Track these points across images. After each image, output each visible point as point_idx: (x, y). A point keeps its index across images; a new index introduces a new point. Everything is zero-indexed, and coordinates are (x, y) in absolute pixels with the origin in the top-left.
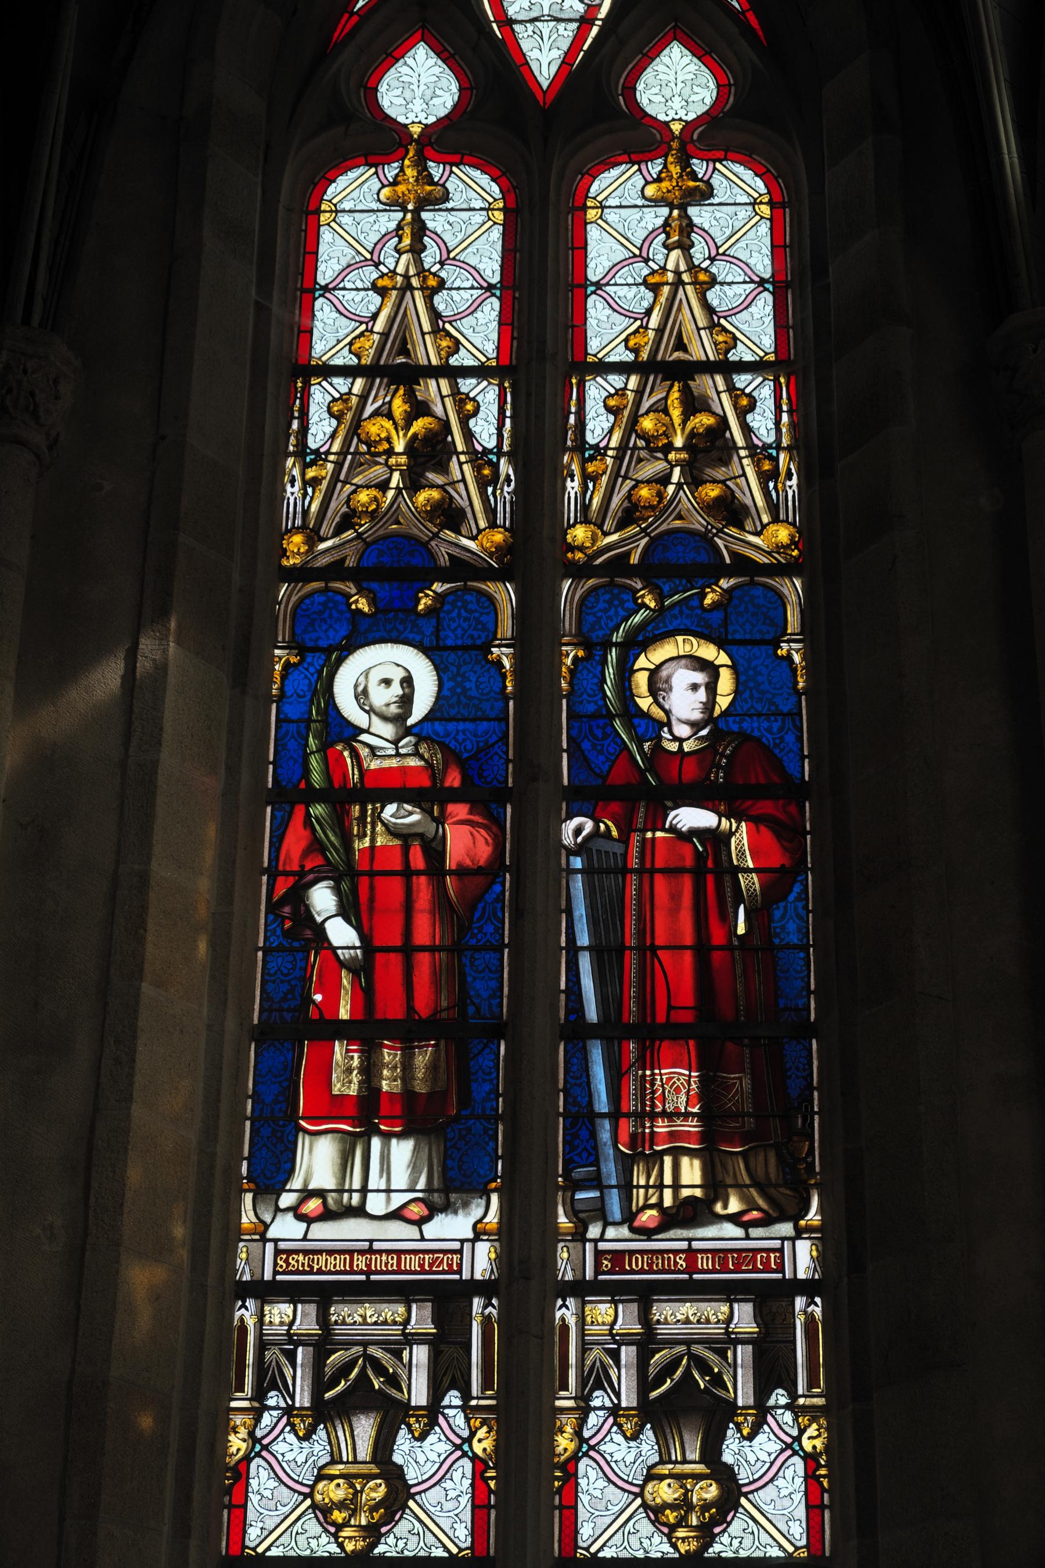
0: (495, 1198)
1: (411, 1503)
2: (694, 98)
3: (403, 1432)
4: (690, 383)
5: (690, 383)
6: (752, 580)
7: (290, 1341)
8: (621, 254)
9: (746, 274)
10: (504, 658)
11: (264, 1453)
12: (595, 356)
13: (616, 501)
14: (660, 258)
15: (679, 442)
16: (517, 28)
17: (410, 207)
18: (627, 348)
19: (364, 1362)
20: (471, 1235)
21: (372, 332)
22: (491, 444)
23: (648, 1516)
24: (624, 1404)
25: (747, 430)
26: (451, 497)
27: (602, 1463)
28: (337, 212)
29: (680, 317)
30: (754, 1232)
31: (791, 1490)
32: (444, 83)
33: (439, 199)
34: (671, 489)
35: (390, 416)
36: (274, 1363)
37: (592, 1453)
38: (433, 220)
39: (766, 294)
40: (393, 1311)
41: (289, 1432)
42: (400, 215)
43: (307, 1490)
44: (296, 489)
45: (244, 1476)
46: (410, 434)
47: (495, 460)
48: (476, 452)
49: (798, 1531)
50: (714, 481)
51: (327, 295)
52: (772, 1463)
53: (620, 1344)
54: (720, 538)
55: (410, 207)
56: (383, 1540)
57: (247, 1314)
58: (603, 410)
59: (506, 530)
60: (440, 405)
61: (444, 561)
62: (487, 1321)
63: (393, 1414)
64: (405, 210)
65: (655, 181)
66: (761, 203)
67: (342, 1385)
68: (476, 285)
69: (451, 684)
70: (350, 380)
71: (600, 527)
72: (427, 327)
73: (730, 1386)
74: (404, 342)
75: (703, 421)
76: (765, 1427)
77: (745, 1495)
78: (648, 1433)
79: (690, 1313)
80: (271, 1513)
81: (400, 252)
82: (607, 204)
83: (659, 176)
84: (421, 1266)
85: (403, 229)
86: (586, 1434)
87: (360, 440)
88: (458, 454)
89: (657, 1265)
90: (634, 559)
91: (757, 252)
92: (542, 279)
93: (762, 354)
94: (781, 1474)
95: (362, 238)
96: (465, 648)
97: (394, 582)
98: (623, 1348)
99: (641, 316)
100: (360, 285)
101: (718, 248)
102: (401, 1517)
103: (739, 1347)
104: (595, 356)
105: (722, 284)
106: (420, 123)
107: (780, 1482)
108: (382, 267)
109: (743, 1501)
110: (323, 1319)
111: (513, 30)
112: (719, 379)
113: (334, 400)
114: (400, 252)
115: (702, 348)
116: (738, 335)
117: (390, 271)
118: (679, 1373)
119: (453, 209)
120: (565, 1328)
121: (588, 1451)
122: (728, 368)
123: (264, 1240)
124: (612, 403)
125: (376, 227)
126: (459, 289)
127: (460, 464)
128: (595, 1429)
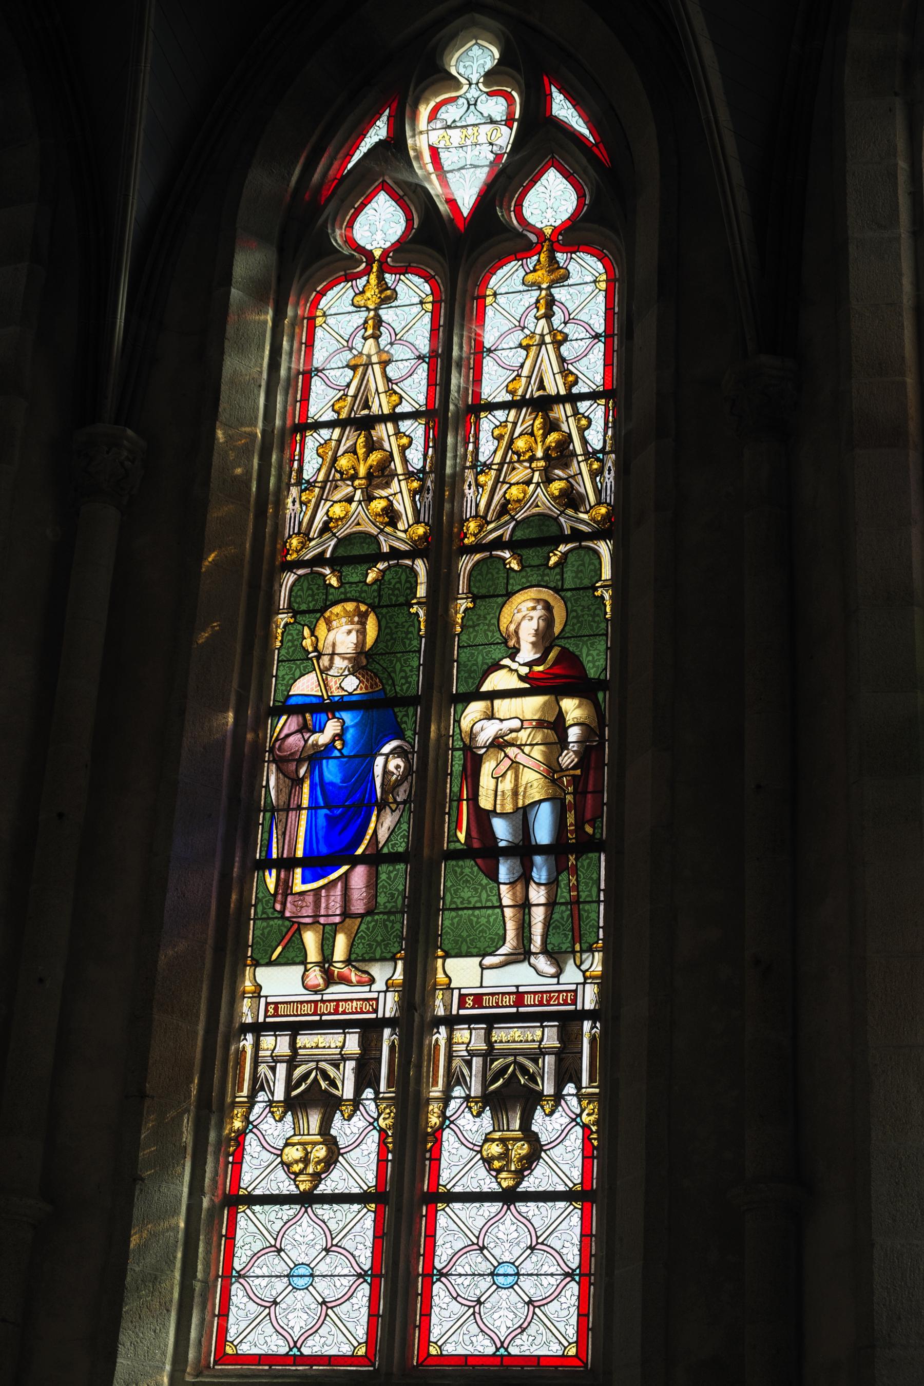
0: (400, 964)
1: (340, 1158)
3: (338, 1115)
13: (496, 498)
15: (539, 454)
18: (333, 410)
20: (582, 981)
21: (347, 395)
24: (472, 1095)
25: (584, 442)
26: (572, 485)
32: (567, 195)
36: (263, 1075)
43: (279, 1152)
44: (472, 490)
48: (589, 453)
50: (381, 498)
51: (320, 374)
52: (563, 1131)
53: (276, 1062)
55: (544, 286)
59: (609, 504)
61: (385, 549)
63: (329, 1104)
64: (540, 289)
65: (531, 272)
67: (303, 1087)
69: (411, 629)
70: (507, 412)
72: (556, 370)
74: (542, 381)
78: (487, 1113)
79: (517, 1035)
81: (365, 339)
83: (534, 268)
86: (251, 1118)
87: (513, 453)
88: (577, 456)
90: (328, 555)
98: (474, 1059)
103: (547, 1057)
108: (354, 351)
109: (543, 1154)
110: (293, 1045)
112: (568, 407)
114: (365, 339)
116: (580, 375)
119: (568, 285)
122: (572, 399)
123: (260, 997)
125: (522, 303)
126: (577, 340)
127: (579, 463)
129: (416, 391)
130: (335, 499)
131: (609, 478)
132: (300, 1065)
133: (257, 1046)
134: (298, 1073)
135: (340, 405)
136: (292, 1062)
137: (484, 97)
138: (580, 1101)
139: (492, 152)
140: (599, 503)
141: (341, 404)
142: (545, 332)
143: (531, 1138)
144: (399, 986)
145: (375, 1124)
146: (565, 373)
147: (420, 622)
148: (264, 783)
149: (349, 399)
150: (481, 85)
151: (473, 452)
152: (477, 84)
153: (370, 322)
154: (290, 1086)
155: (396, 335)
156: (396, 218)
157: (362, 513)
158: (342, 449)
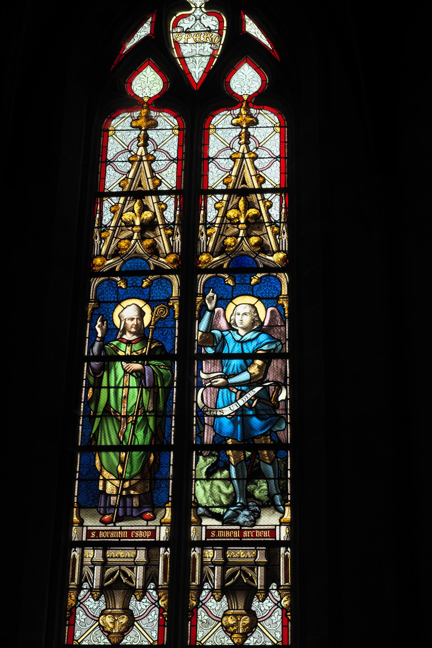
2: (154, 88)
4: (143, 200)
5: (143, 200)
6: (161, 276)
7: (213, 564)
8: (120, 149)
9: (167, 156)
10: (284, 302)
11: (203, 606)
12: (108, 189)
13: (112, 246)
14: (135, 150)
15: (242, 220)
16: (186, 59)
17: (143, 128)
18: (120, 186)
19: (240, 572)
20: (159, 524)
22: (277, 219)
23: (100, 629)
26: (263, 240)
27: (85, 609)
28: (115, 130)
29: (244, 171)
30: (150, 523)
31: (277, 620)
33: (154, 125)
34: (133, 242)
35: (133, 211)
36: (86, 572)
37: (203, 606)
38: (151, 134)
39: (277, 162)
40: (130, 553)
41: (212, 599)
42: (240, 130)
45: (74, 613)
46: (246, 216)
47: (173, 227)
49: (154, 634)
50: (256, 236)
53: (95, 565)
54: (151, 260)
56: (125, 638)
57: (76, 554)
58: (214, 209)
60: (152, 206)
62: (286, 558)
64: (242, 128)
66: (175, 129)
68: (167, 159)
70: (119, 198)
71: (212, 255)
72: (149, 176)
73: (134, 581)
74: (140, 182)
75: (252, 212)
76: (268, 597)
77: (136, 621)
78: (225, 598)
79: (121, 554)
80: (84, 628)
82: (218, 127)
84: (263, 535)
85: (241, 135)
88: (265, 223)
89: (235, 535)
90: (225, 266)
91: (274, 145)
92: (193, 157)
93: (275, 185)
94: (273, 614)
95: (226, 139)
96: (107, 302)
97: (136, 276)
99: (229, 171)
100: (123, 160)
101: (157, 146)
102: (132, 630)
104: (211, 187)
105: (260, 158)
106: (247, 94)
107: (273, 618)
108: (233, 150)
110: (224, 555)
111: (185, 60)
113: (113, 206)
114: (240, 144)
115: (252, 183)
117: (237, 151)
118: (116, 576)
120: (195, 559)
121: (202, 605)
122: (263, 191)
124: (217, 206)
125: (130, 137)
126: (161, 160)
128: (83, 596)
129: (170, 178)
130: (121, 237)
131: (178, 239)
132: (109, 568)
133: (202, 555)
134: (108, 572)
135: (227, 180)
136: (104, 565)
137: (205, 15)
138: (157, 593)
139: (211, 48)
140: (171, 253)
141: (125, 182)
142: (143, 155)
143: (252, 614)
144: (169, 523)
145: (157, 604)
146: (258, 176)
147: (174, 311)
148: (195, 400)
149: (129, 180)
150: (203, 9)
151: (99, 219)
152: (200, 7)
153: (243, 135)
154: (103, 579)
155: (259, 144)
156: (138, 81)
157: (138, 247)
158: (230, 206)
